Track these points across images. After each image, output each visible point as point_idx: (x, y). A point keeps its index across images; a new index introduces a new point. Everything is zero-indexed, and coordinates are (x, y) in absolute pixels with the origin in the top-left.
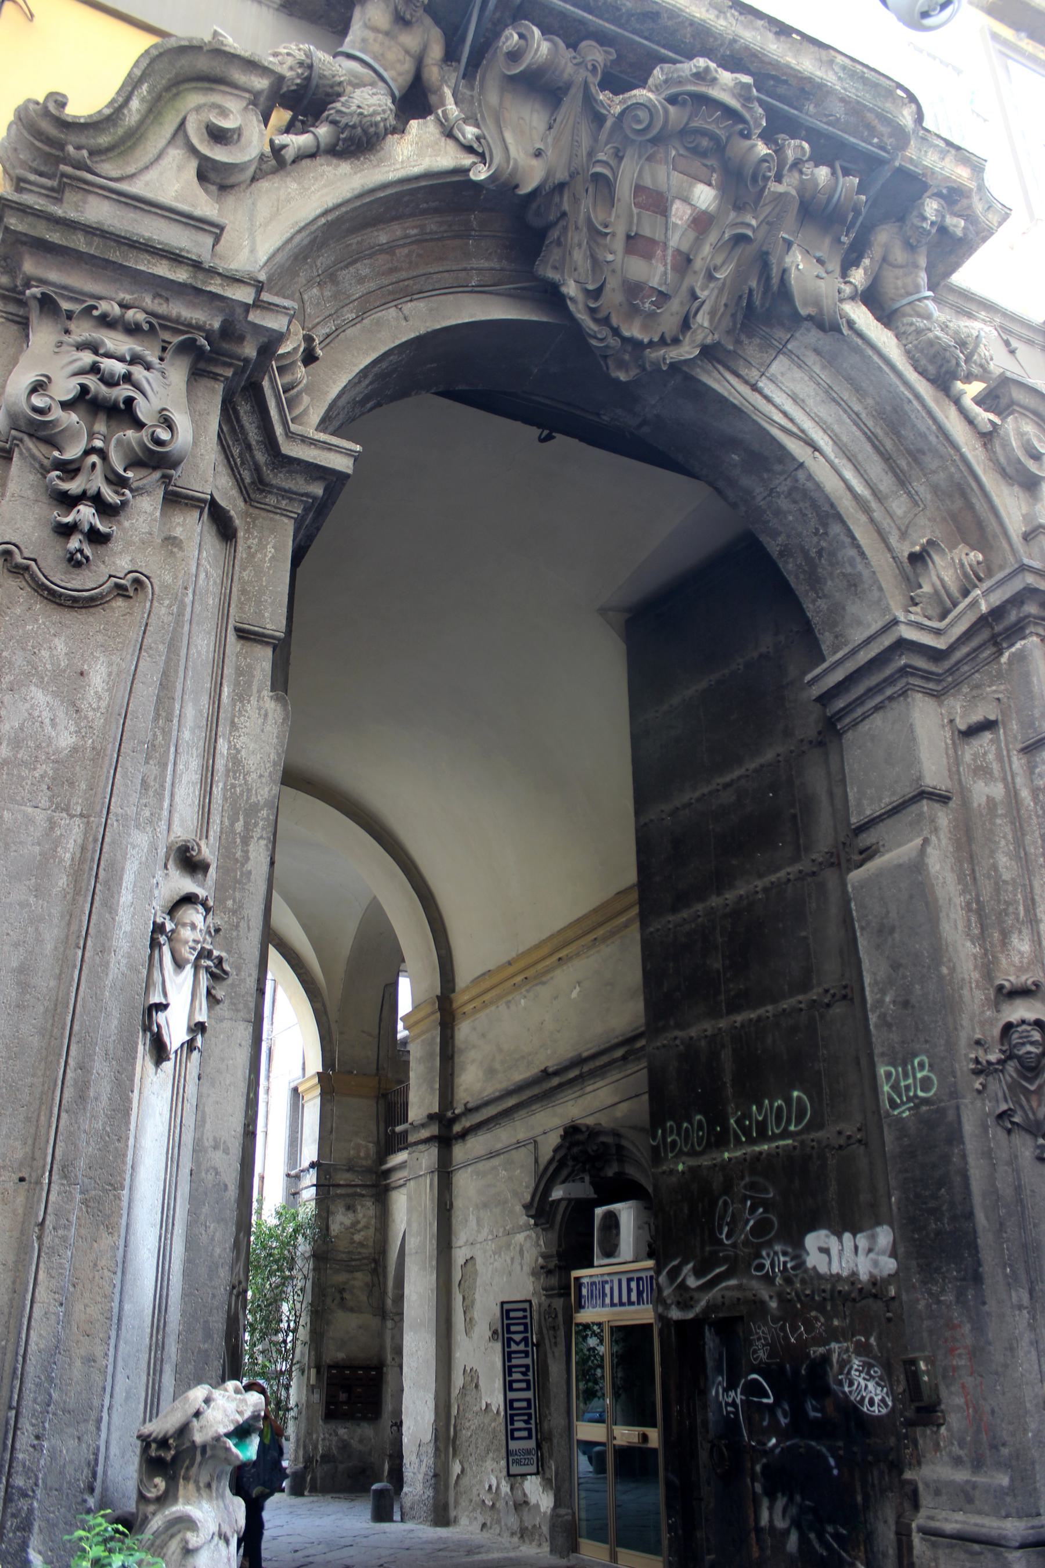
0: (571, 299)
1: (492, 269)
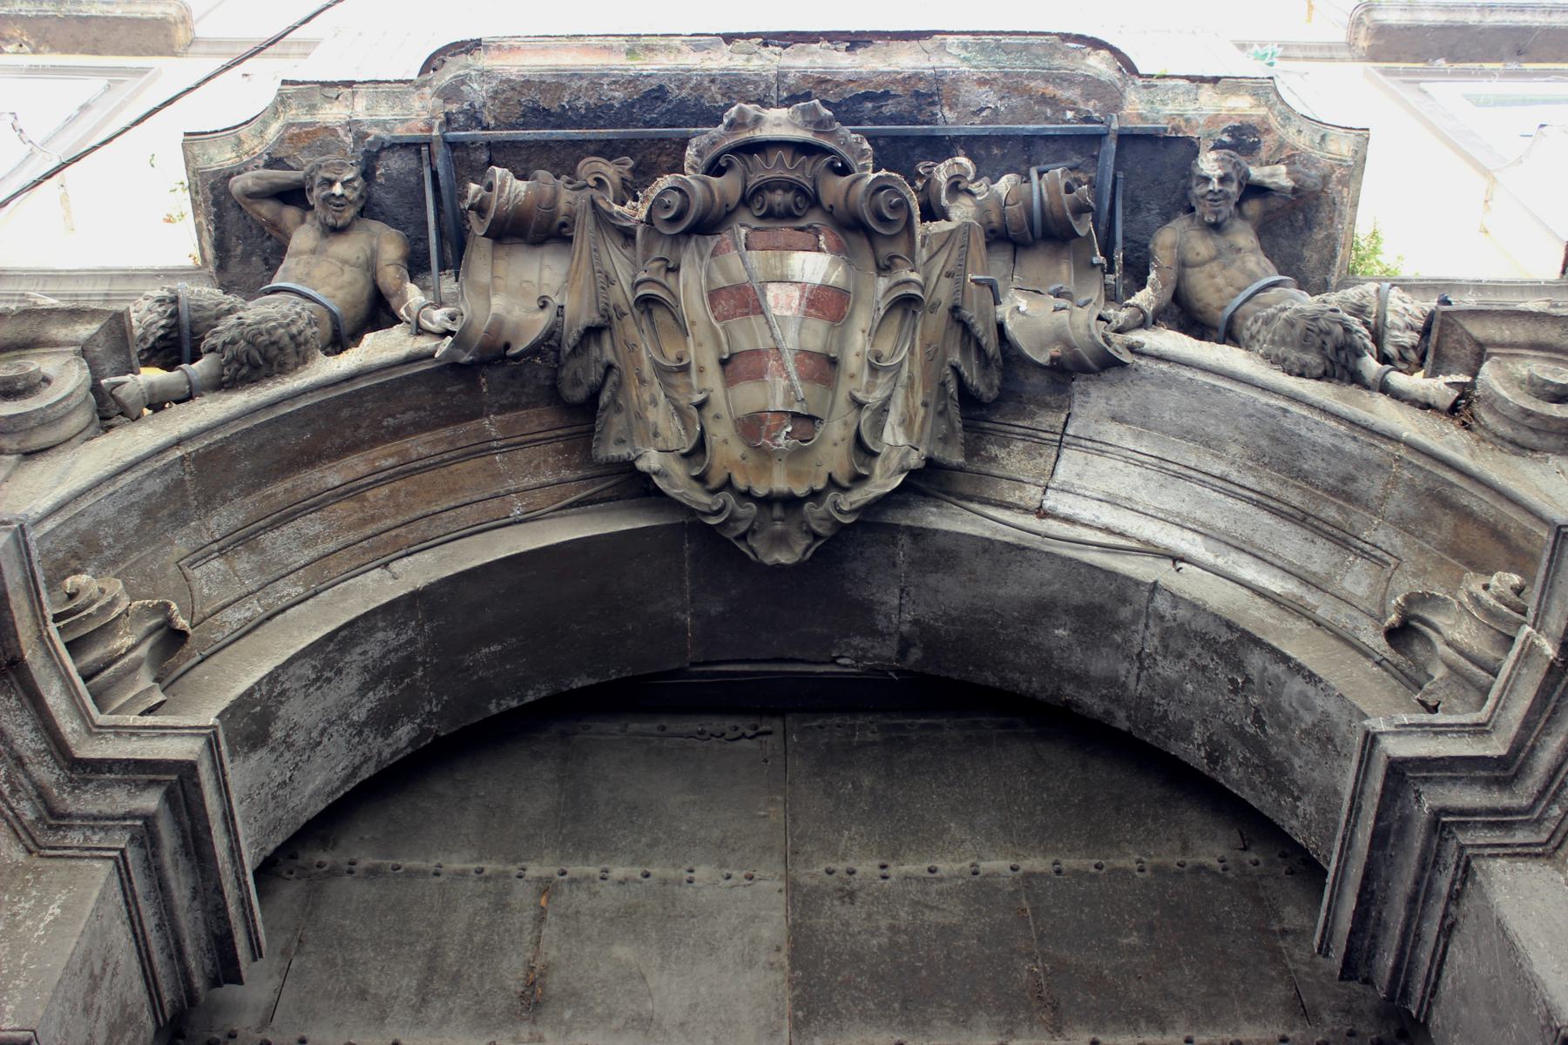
0: (656, 473)
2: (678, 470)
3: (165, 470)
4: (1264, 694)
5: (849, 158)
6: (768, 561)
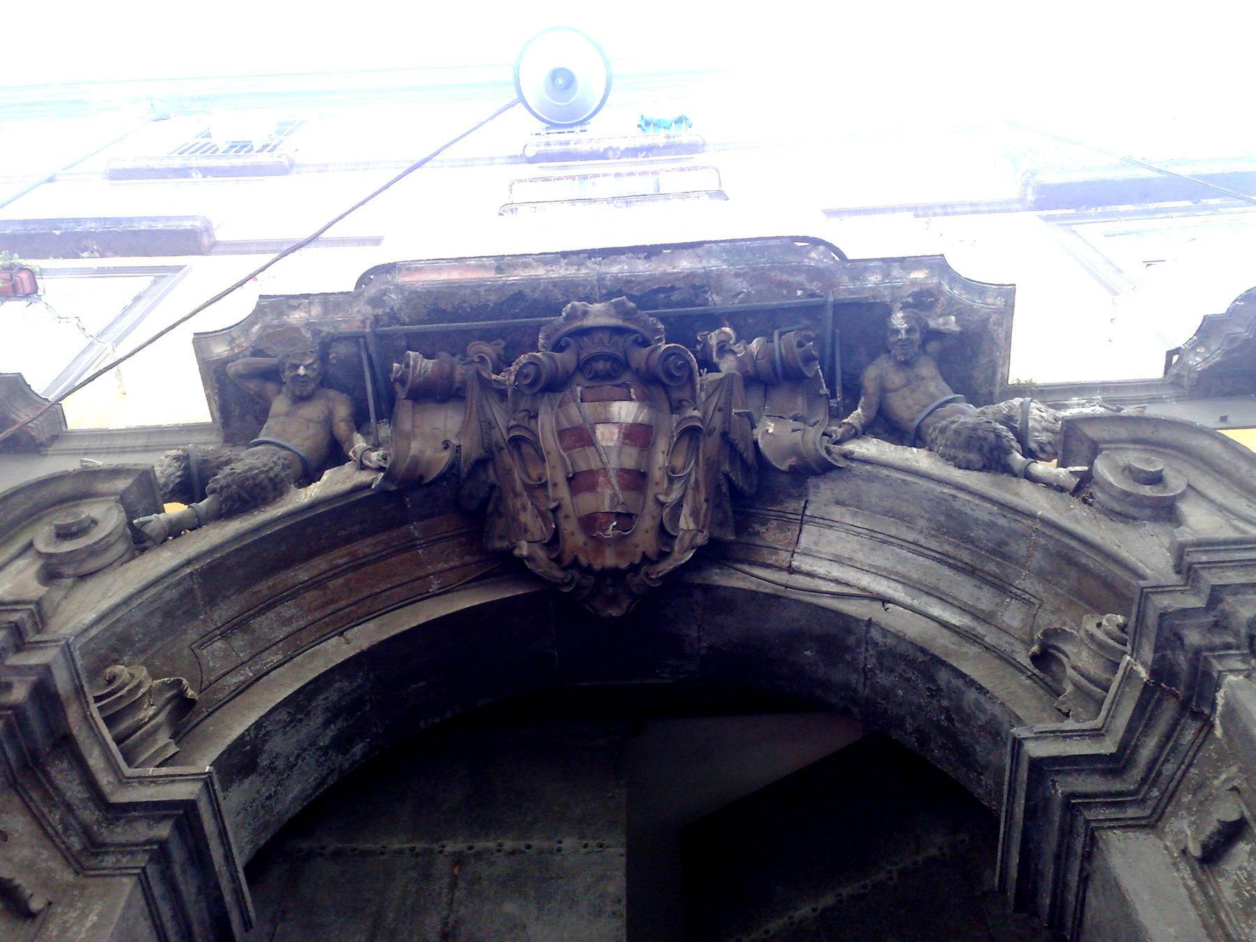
1: (451, 569)
2: (541, 554)
3: (179, 583)
4: (950, 699)
5: (647, 334)
6: (604, 614)
